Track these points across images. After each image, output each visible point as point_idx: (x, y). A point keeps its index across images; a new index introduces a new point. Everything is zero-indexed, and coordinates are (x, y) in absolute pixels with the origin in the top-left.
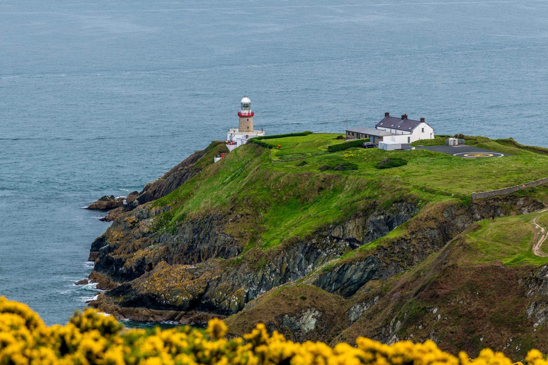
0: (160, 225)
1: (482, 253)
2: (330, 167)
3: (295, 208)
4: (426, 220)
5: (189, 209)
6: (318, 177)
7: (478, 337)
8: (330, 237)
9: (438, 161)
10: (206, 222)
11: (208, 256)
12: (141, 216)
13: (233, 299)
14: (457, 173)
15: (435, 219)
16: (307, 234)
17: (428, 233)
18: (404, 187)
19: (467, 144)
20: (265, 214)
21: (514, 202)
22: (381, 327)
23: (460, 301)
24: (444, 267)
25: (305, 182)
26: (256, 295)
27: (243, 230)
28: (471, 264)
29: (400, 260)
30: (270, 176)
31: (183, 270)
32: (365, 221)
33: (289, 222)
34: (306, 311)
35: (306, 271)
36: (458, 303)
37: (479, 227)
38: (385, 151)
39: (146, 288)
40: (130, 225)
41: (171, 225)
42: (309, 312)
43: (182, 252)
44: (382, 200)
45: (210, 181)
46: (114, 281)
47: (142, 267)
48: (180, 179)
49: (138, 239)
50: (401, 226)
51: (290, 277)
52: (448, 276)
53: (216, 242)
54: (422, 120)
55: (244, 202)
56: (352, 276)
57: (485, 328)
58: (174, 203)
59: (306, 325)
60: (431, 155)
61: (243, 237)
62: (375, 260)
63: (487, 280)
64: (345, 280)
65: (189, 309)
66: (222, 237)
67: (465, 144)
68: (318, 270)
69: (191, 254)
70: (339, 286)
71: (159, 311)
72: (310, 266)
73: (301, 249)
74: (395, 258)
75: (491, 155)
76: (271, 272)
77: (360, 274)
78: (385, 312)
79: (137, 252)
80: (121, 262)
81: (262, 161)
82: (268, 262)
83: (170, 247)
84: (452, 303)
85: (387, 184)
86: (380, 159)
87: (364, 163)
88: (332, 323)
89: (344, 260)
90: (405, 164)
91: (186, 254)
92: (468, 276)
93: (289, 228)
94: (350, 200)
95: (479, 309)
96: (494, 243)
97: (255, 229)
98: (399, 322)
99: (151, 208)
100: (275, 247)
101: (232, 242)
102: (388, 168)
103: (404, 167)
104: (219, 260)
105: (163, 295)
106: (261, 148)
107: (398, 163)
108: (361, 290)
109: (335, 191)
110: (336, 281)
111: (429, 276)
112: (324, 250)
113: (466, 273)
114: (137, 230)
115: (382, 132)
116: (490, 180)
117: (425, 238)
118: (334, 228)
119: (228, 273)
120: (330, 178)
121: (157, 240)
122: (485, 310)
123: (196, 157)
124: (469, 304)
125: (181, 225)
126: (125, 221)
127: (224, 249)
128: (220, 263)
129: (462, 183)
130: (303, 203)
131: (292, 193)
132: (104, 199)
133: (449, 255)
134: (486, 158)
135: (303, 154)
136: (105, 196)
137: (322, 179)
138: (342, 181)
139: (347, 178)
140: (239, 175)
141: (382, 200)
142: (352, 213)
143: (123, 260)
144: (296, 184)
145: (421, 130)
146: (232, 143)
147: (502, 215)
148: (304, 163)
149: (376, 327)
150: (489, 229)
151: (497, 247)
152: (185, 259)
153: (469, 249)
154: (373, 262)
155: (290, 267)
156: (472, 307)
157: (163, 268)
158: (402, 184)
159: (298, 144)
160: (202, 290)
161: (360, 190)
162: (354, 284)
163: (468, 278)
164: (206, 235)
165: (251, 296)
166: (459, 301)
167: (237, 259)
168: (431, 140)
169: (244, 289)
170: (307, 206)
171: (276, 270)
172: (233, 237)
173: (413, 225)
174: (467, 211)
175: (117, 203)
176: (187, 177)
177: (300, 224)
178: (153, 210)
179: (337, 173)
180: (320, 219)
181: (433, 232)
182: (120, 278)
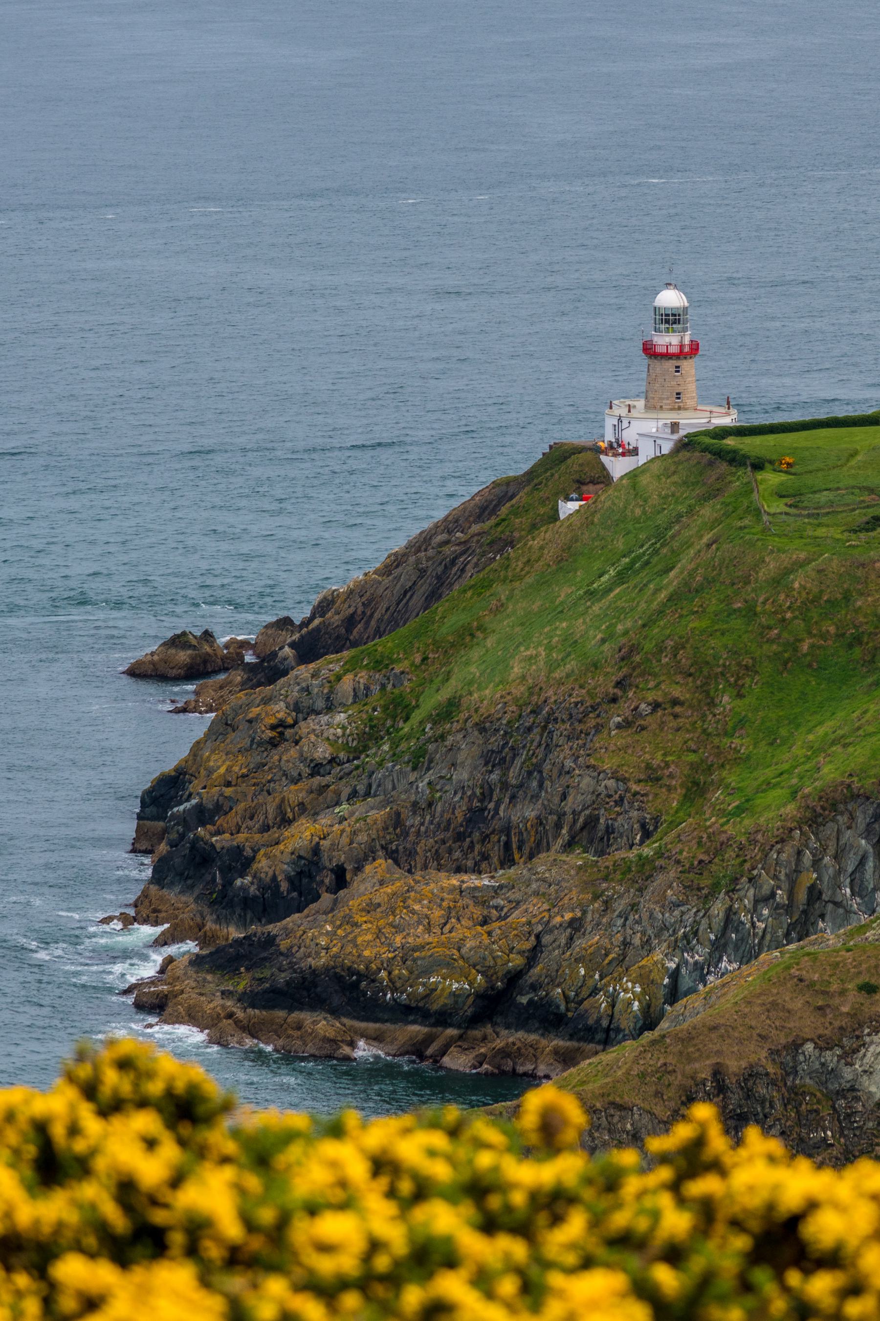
0: (369, 736)
5: (471, 683)
10: (529, 729)
11: (538, 844)
12: (306, 702)
13: (626, 991)
20: (738, 702)
27: (659, 756)
30: (755, 567)
33: (821, 731)
39: (327, 949)
41: (408, 737)
43: (447, 829)
46: (218, 921)
47: (311, 877)
48: (438, 577)
49: (296, 781)
51: (822, 916)
53: (564, 797)
55: (665, 660)
58: (418, 660)
61: (658, 779)
65: (475, 1020)
66: (587, 780)
69: (478, 836)
73: (861, 821)
76: (756, 902)
79: (293, 829)
80: (240, 860)
81: (727, 515)
82: (747, 866)
83: (405, 813)
91: (459, 837)
99: (339, 678)
100: (771, 815)
101: (622, 799)
104: (577, 858)
105: (383, 974)
114: (293, 752)
119: (606, 902)
125: (443, 737)
126: (250, 721)
127: (592, 822)
128: (580, 868)
131: (832, 629)
132: (178, 641)
136: (184, 634)
140: (647, 563)
143: (248, 852)
144: (847, 597)
146: (620, 449)
152: (457, 854)
155: (824, 885)
157: (382, 883)
159: (854, 454)
160: (516, 961)
164: (530, 773)
165: (686, 981)
167: (640, 856)
169: (662, 959)
171: (773, 895)
172: (625, 780)
175: (224, 658)
176: (463, 570)
178: (347, 684)
182: (238, 911)
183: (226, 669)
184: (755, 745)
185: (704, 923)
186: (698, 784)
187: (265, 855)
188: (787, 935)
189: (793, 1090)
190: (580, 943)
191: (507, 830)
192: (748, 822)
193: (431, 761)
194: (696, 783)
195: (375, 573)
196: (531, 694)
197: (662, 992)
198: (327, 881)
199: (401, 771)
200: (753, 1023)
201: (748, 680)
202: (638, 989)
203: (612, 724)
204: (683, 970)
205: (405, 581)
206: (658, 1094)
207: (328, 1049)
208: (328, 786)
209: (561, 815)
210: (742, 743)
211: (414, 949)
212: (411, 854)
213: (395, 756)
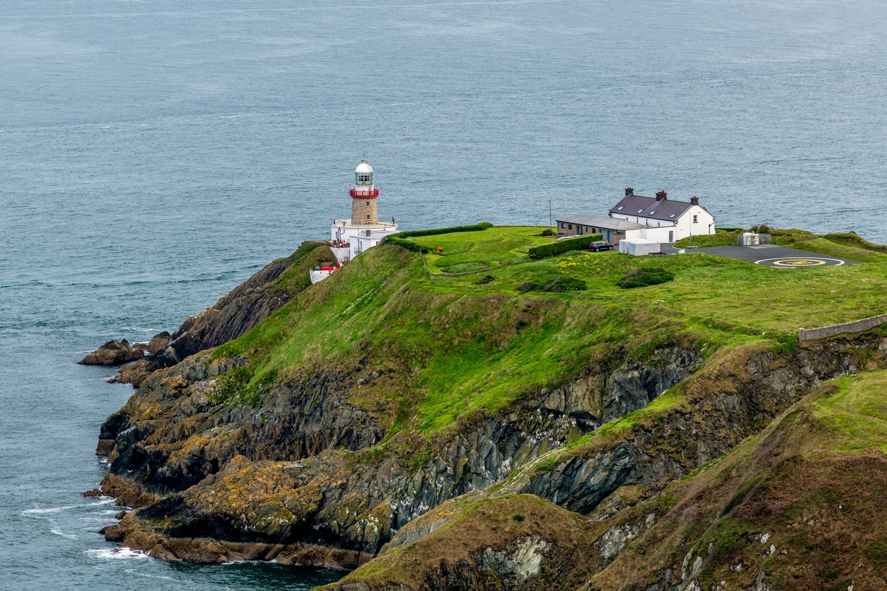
0: (228, 391)
1: (844, 435)
2: (536, 286)
3: (477, 359)
4: (717, 378)
5: (282, 363)
6: (515, 303)
7: (843, 584)
8: (542, 410)
9: (729, 273)
10: (315, 386)
11: (321, 445)
12: (193, 375)
13: (370, 521)
14: (766, 295)
15: (733, 376)
16: (500, 405)
17: (722, 401)
18: (674, 319)
19: (775, 243)
20: (423, 370)
21: (873, 345)
22: (664, 569)
23: (810, 520)
24: (775, 461)
25: (493, 313)
26: (411, 514)
27: (384, 398)
28: (827, 456)
29: (673, 449)
30: (429, 302)
31: (278, 471)
32: (605, 381)
33: (467, 385)
35: (499, 470)
36: (806, 524)
37: (835, 389)
38: (631, 257)
39: (213, 503)
40: (174, 391)
41: (249, 391)
42: (528, 542)
43: (271, 438)
44: (633, 343)
45: (317, 311)
46: (149, 491)
47: (200, 466)
48: (248, 310)
49: (189, 416)
50: (673, 388)
51: (471, 481)
52: (787, 476)
53: (334, 420)
54: (694, 201)
55: (385, 350)
56: (588, 478)
57: (856, 569)
58: (252, 352)
59: (524, 566)
60: (716, 263)
61: (383, 410)
62: (630, 450)
63: (857, 484)
64: (576, 486)
65: (289, 541)
66: (346, 411)
67: (771, 243)
68: (527, 469)
69: (288, 442)
70: (566, 496)
71: (237, 544)
72: (507, 462)
73: (490, 431)
74: (665, 447)
75: (822, 263)
76: (437, 473)
77: (602, 475)
78: (671, 542)
79: (189, 441)
80: (160, 458)
81: (412, 276)
82: (432, 454)
83: (249, 430)
84: (795, 525)
85: (643, 315)
86: (625, 271)
87: (596, 279)
88: (569, 563)
89: (574, 451)
90: (670, 279)
91: (278, 442)
92: (823, 476)
93: (468, 394)
94: (576, 343)
95: (843, 535)
96: (864, 417)
97: (407, 397)
98: (699, 558)
99: (210, 362)
100: (444, 428)
101: (365, 420)
102: (641, 286)
103: (669, 285)
104: (342, 452)
105: (243, 516)
106: (407, 252)
107: (659, 277)
108: (605, 504)
109: (547, 327)
110: (560, 488)
111: (748, 477)
112: (531, 433)
113: (817, 471)
114: (187, 401)
115: (622, 223)
116: (827, 307)
117: (716, 410)
118: (550, 393)
119: (359, 475)
120: (537, 305)
121: (225, 418)
122: (854, 536)
123: (275, 271)
124: (826, 525)
125: (268, 391)
126: (162, 385)
127: (349, 433)
128: (345, 457)
129: (779, 312)
130: (491, 349)
131: (469, 333)
132: (110, 345)
133: (783, 440)
134: (814, 268)
135: (484, 263)
136: (113, 341)
137: (524, 307)
138: (560, 309)
139: (568, 305)
140: (371, 301)
141: (633, 343)
142: (580, 367)
143: (165, 454)
144: (476, 316)
145: (693, 218)
146: (340, 244)
147: (852, 368)
148: (489, 279)
149: (654, 568)
150: (854, 393)
151: (870, 424)
152: (277, 451)
153: (820, 428)
154: (626, 453)
155: (471, 465)
156: (830, 531)
157: (240, 468)
158: (669, 315)
159: (472, 245)
160: (313, 507)
161: (593, 326)
162: (593, 492)
163: (823, 479)
164: (315, 408)
165: (402, 516)
166: (807, 521)
167: (376, 450)
168: (711, 237)
169: (389, 504)
170: (497, 355)
171: (446, 470)
172: (366, 411)
173: (694, 388)
174: (790, 362)
175: (134, 353)
176: (261, 306)
177: (488, 386)
178: (215, 365)
179: (551, 295)
180: (524, 378)
181: (730, 399)
182: (160, 485)
183: (136, 360)
184: (433, 392)
185: (411, 485)
186: (404, 412)
187: (175, 455)
188: (453, 491)
189: (481, 573)
190: (346, 496)
191: (303, 438)
192: (432, 432)
193: (262, 403)
194: (403, 412)
195: (214, 308)
196: (315, 368)
197: (390, 522)
198: (208, 467)
199: (246, 409)
200: (460, 537)
201: (427, 359)
202: (377, 520)
203: (358, 382)
204: (400, 510)
205: (231, 312)
206: (413, 576)
207: (213, 558)
208: (207, 418)
209: (333, 430)
210: (426, 391)
211: (259, 502)
212: (253, 452)
213: (243, 401)
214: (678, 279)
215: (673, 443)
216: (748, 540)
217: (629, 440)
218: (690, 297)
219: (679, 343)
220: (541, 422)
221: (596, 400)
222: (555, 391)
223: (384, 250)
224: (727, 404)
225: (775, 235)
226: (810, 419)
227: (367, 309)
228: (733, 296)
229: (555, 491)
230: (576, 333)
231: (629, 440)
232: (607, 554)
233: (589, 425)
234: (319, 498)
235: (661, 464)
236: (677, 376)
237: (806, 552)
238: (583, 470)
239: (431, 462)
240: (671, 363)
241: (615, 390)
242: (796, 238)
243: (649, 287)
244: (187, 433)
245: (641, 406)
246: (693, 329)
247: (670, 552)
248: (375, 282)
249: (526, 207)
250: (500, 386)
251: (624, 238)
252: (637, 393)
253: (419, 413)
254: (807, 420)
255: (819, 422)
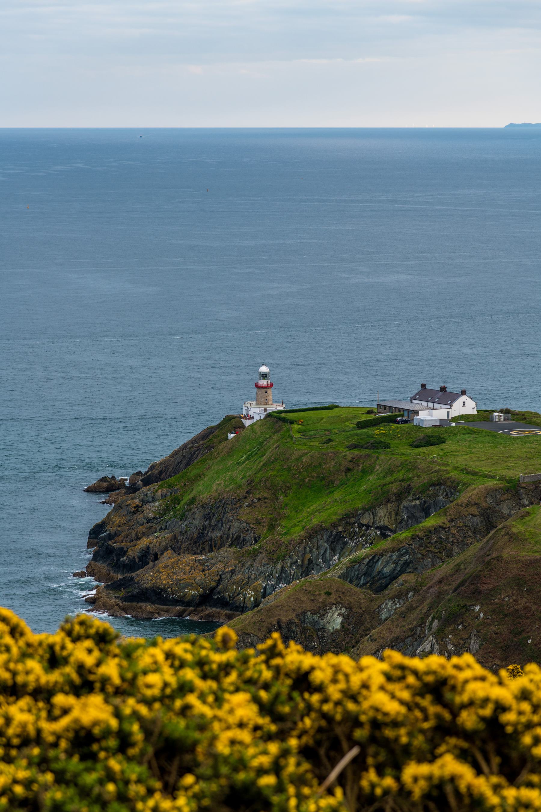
0: (166, 510)
1: (530, 543)
4: (467, 505)
5: (199, 492)
6: (345, 456)
8: (358, 524)
10: (218, 507)
11: (221, 545)
12: (146, 499)
13: (249, 594)
19: (514, 420)
20: (285, 498)
22: (416, 627)
24: (487, 559)
25: (330, 463)
26: (274, 590)
27: (260, 516)
28: (518, 556)
30: (291, 455)
32: (398, 506)
33: (312, 508)
34: (331, 608)
35: (331, 562)
36: (503, 600)
37: (528, 514)
38: (421, 427)
39: (151, 581)
42: (334, 609)
44: (417, 483)
46: (114, 572)
47: (146, 557)
48: (189, 458)
49: (142, 525)
50: (439, 512)
51: (313, 569)
52: (492, 569)
53: (229, 529)
54: (464, 393)
55: (262, 485)
56: (383, 568)
57: (534, 629)
58: (183, 485)
59: (331, 624)
60: (474, 432)
61: (260, 523)
62: (409, 551)
63: (536, 575)
64: (375, 573)
65: (199, 604)
66: (237, 523)
67: (512, 420)
68: (345, 562)
69: (201, 543)
70: (369, 579)
71: (165, 607)
72: (336, 557)
74: (432, 549)
76: (291, 564)
78: (421, 610)
79: (140, 541)
80: (123, 552)
81: (282, 438)
82: (288, 552)
83: (178, 535)
84: (497, 600)
85: (423, 465)
86: (415, 436)
90: (444, 442)
91: (195, 543)
93: (312, 514)
98: (436, 621)
99: (157, 491)
100: (296, 535)
101: (248, 530)
102: (425, 446)
103: (443, 446)
104: (233, 549)
105: (169, 589)
106: (281, 423)
107: (436, 441)
111: (470, 569)
112: (352, 539)
114: (141, 515)
117: (466, 526)
119: (243, 564)
121: (163, 527)
122: (534, 608)
124: (516, 601)
125: (190, 510)
126: (127, 505)
127: (238, 537)
128: (234, 553)
129: (509, 464)
130: (328, 485)
131: (315, 475)
132: (104, 479)
134: (536, 436)
135: (328, 430)
136: (105, 477)
137: (350, 459)
138: (373, 460)
139: (378, 458)
140: (256, 453)
141: (417, 483)
142: (383, 497)
143: (125, 549)
144: (320, 464)
148: (330, 440)
149: (410, 626)
152: (195, 548)
153: (515, 539)
154: (407, 553)
155: (313, 558)
157: (170, 558)
159: (323, 418)
160: (213, 584)
161: (392, 471)
162: (386, 577)
164: (218, 521)
165: (269, 590)
166: (504, 598)
167: (254, 549)
168: (473, 415)
169: (261, 583)
170: (332, 489)
171: (297, 561)
172: (249, 524)
175: (119, 485)
176: (197, 456)
177: (325, 509)
178: (159, 493)
179: (367, 451)
180: (347, 504)
181: (475, 519)
182: (121, 569)
184: (291, 512)
185: (275, 571)
188: (301, 575)
189: (304, 628)
190: (234, 578)
191: (211, 540)
192: (289, 537)
193: (186, 518)
194: (272, 525)
196: (219, 496)
197: (261, 594)
198: (151, 558)
200: (291, 605)
201: (288, 491)
202: (253, 593)
204: (268, 587)
205: (179, 460)
206: (259, 629)
209: (228, 535)
210: (286, 511)
212: (180, 548)
213: (175, 516)
214: (449, 442)
215: (436, 546)
216: (467, 610)
217: (409, 545)
218: (455, 453)
219: (444, 483)
220: (357, 532)
221: (393, 519)
222: (367, 513)
223: (267, 421)
224: (473, 522)
225: (514, 415)
226: (510, 533)
227: (253, 459)
228: (482, 454)
229: (362, 576)
230: (381, 475)
231: (409, 545)
232: (383, 617)
233: (388, 535)
234: (217, 578)
235: (430, 560)
236: (443, 504)
237: (503, 618)
238: (380, 564)
239: (287, 556)
240: (439, 496)
241: (405, 513)
242: (527, 417)
243: (430, 447)
244: (140, 536)
245: (420, 522)
246: (454, 474)
247: (420, 616)
248: (260, 442)
249: (357, 394)
250: (333, 509)
251: (418, 416)
252: (418, 515)
253: (282, 526)
254: (507, 534)
255: (515, 534)
